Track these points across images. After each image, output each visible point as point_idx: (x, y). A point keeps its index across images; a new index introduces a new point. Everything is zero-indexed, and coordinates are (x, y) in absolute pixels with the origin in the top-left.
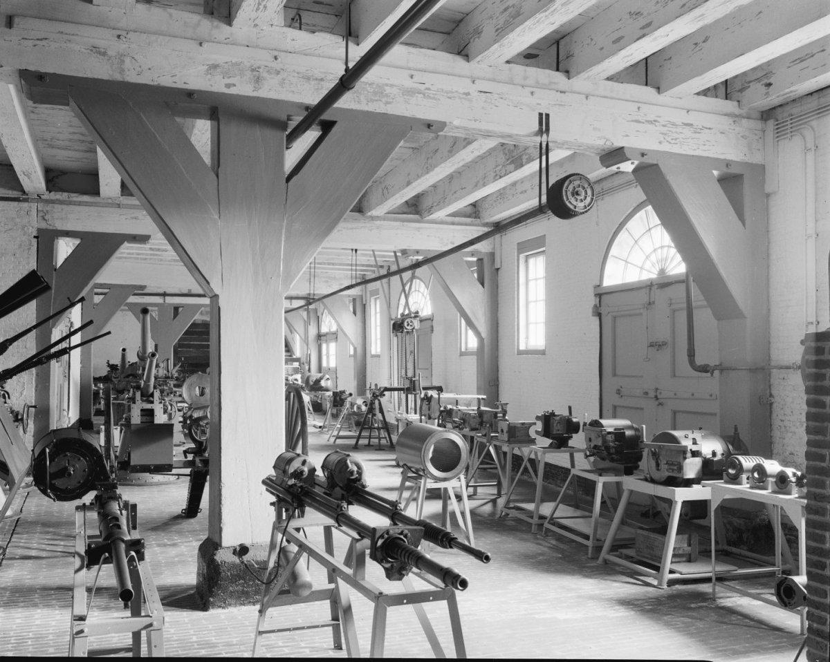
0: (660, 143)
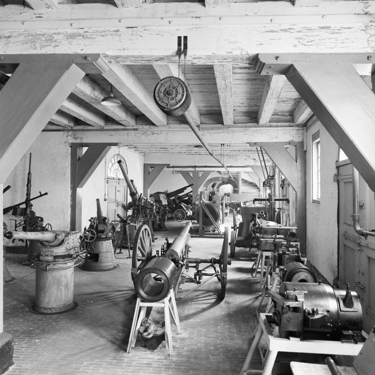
0: (295, 46)
